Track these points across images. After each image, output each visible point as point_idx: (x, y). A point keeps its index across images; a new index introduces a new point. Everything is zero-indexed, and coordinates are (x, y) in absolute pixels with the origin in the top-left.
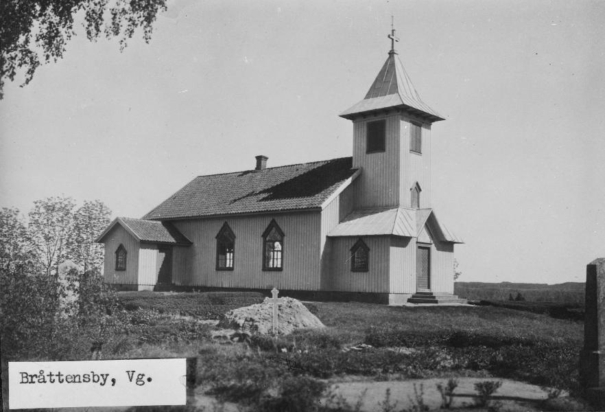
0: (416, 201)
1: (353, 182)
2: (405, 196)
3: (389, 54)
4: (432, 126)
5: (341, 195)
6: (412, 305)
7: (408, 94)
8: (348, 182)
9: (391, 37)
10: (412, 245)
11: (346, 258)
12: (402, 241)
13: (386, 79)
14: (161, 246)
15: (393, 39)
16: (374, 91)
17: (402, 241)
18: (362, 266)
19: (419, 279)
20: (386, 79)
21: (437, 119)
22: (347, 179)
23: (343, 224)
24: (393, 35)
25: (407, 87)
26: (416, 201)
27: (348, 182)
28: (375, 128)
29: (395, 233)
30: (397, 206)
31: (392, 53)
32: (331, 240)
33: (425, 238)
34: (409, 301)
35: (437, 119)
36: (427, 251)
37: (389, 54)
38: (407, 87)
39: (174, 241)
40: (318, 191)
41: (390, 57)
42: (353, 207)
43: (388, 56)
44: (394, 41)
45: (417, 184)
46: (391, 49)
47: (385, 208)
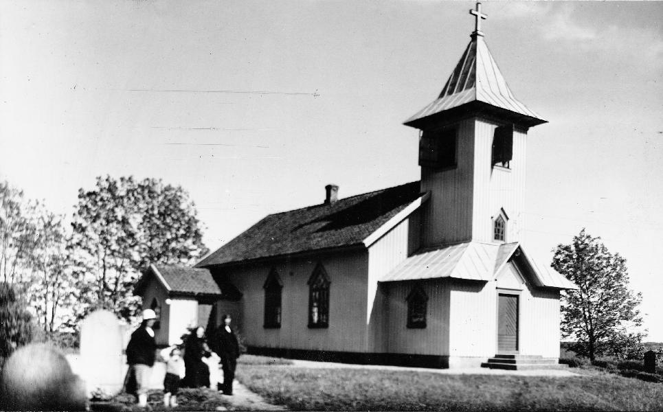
0: (499, 233)
1: (423, 204)
2: (481, 225)
3: (471, 36)
4: (528, 132)
5: (410, 217)
6: (487, 371)
7: (491, 87)
8: (416, 204)
9: (473, 12)
10: (489, 292)
11: (401, 306)
12: (475, 285)
13: (464, 73)
14: (202, 299)
15: (476, 16)
16: (450, 88)
17: (475, 285)
18: (417, 321)
19: (501, 337)
20: (464, 73)
21: (536, 122)
22: (416, 199)
23: (416, 258)
24: (477, 10)
25: (492, 78)
26: (499, 233)
27: (416, 204)
28: (442, 139)
29: (453, 276)
30: (468, 239)
31: (474, 36)
32: (386, 288)
33: (512, 280)
34: (484, 365)
35: (536, 122)
36: (516, 299)
37: (471, 36)
38: (492, 78)
39: (218, 292)
40: (364, 221)
41: (472, 41)
42: (420, 242)
43: (470, 39)
44: (479, 18)
45: (502, 209)
46: (474, 30)
47: (456, 242)
